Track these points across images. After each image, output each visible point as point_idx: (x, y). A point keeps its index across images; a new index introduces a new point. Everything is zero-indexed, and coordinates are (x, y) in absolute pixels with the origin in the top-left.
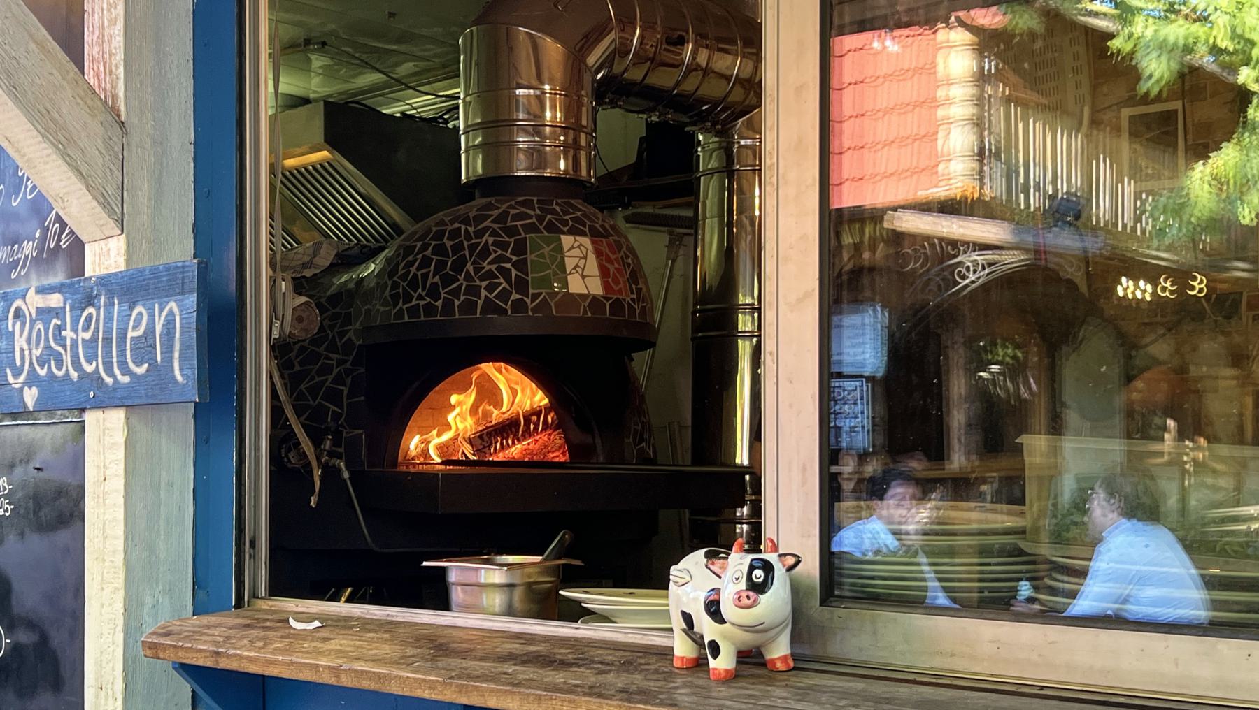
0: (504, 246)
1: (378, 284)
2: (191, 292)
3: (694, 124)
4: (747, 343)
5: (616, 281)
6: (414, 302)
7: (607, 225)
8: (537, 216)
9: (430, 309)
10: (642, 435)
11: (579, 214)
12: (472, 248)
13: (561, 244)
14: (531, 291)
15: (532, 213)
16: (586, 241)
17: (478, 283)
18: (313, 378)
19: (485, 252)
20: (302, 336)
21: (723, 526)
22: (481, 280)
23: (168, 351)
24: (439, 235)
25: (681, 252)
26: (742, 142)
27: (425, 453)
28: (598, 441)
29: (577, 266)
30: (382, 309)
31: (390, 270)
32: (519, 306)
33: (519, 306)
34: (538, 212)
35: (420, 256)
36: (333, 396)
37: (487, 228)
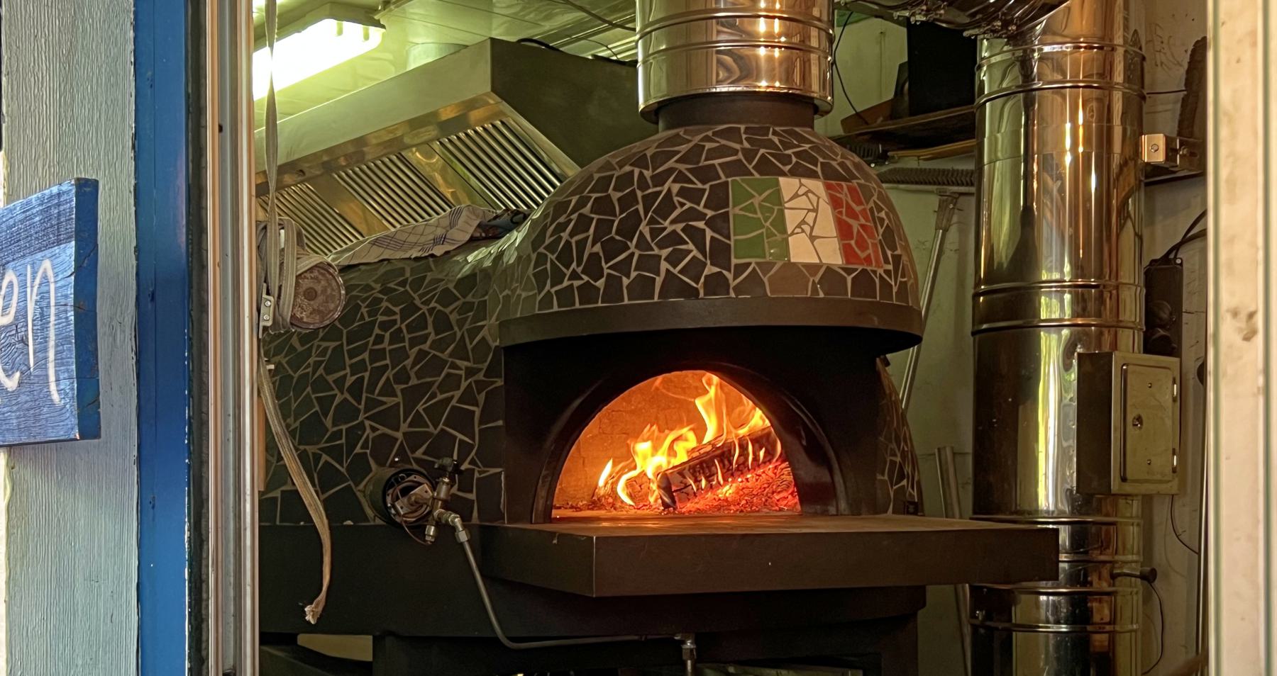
0: (694, 196)
1: (519, 258)
2: (68, 240)
3: (976, 25)
4: (1054, 336)
6: (566, 283)
7: (848, 163)
8: (744, 150)
10: (901, 468)
11: (807, 146)
12: (649, 200)
13: (778, 192)
14: (734, 261)
15: (737, 146)
16: (817, 186)
17: (656, 251)
18: (433, 396)
19: (667, 206)
21: (1024, 597)
22: (661, 247)
23: (42, 349)
24: (603, 184)
25: (955, 219)
26: (1047, 49)
28: (838, 478)
29: (803, 222)
30: (524, 295)
31: (535, 240)
32: (718, 284)
33: (718, 284)
34: (746, 145)
35: (575, 216)
36: (461, 420)
37: (671, 170)
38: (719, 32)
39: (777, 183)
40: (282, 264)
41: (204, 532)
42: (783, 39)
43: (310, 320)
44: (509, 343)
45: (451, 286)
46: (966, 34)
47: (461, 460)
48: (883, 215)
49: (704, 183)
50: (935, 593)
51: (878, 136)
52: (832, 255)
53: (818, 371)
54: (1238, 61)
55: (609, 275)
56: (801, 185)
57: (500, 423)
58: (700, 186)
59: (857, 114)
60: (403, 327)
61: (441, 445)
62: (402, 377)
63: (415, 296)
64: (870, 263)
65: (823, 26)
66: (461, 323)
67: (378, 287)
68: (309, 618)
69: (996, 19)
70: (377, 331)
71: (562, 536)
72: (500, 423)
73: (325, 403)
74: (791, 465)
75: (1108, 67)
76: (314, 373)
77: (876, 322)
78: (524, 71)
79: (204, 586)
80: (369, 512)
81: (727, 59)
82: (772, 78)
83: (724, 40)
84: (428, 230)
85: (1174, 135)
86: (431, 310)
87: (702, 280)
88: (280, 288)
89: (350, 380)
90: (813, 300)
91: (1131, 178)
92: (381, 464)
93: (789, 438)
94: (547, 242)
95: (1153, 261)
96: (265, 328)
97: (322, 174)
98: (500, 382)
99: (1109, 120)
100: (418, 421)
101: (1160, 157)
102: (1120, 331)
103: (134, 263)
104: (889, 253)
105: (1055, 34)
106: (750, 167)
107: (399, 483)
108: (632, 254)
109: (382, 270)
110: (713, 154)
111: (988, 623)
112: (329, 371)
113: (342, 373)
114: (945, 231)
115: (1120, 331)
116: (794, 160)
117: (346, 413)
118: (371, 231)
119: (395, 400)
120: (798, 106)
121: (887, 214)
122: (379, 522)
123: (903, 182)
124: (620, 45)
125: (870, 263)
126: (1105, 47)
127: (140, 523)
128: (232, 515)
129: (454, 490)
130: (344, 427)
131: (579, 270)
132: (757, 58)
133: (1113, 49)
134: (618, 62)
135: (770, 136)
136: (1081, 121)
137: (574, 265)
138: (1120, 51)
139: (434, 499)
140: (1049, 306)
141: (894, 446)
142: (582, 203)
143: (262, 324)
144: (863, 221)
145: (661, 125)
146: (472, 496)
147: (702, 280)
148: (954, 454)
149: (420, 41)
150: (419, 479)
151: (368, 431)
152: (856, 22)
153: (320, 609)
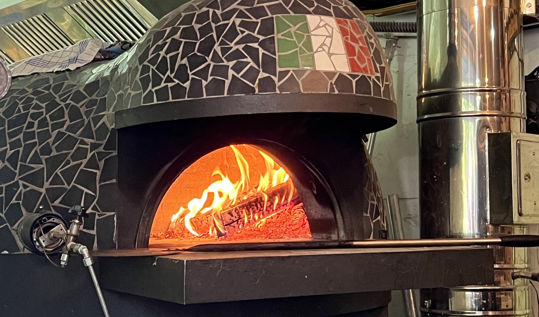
0: (251, 26)
1: (130, 69)
6: (163, 85)
12: (220, 30)
13: (306, 25)
14: (278, 69)
16: (331, 21)
17: (226, 63)
18: (68, 163)
24: (188, 19)
25: (396, 53)
29: (323, 44)
30: (133, 93)
35: (169, 40)
36: (88, 179)
37: (235, 10)
39: (306, 19)
44: (122, 126)
45: (81, 89)
47: (86, 207)
48: (372, 41)
49: (257, 18)
52: (343, 66)
53: (325, 144)
55: (192, 78)
56: (321, 20)
57: (114, 181)
58: (254, 20)
60: (47, 116)
61: (72, 197)
62: (46, 150)
63: (56, 96)
64: (367, 72)
66: (88, 114)
67: (31, 91)
70: (29, 119)
72: (114, 181)
77: (371, 111)
80: (21, 245)
86: (67, 106)
87: (257, 82)
89: (10, 153)
90: (330, 95)
91: (515, 26)
92: (29, 210)
94: (150, 57)
98: (115, 153)
102: (512, 119)
104: (378, 65)
106: (288, 8)
108: (209, 65)
109: (33, 80)
111: (434, 311)
115: (512, 119)
119: (42, 166)
121: (375, 41)
122: (27, 251)
125: (367, 72)
131: (172, 76)
137: (168, 73)
139: (68, 235)
141: (372, 194)
142: (174, 32)
144: (361, 44)
146: (94, 232)
147: (257, 82)
148: (399, 199)
150: (56, 220)
151: (21, 188)
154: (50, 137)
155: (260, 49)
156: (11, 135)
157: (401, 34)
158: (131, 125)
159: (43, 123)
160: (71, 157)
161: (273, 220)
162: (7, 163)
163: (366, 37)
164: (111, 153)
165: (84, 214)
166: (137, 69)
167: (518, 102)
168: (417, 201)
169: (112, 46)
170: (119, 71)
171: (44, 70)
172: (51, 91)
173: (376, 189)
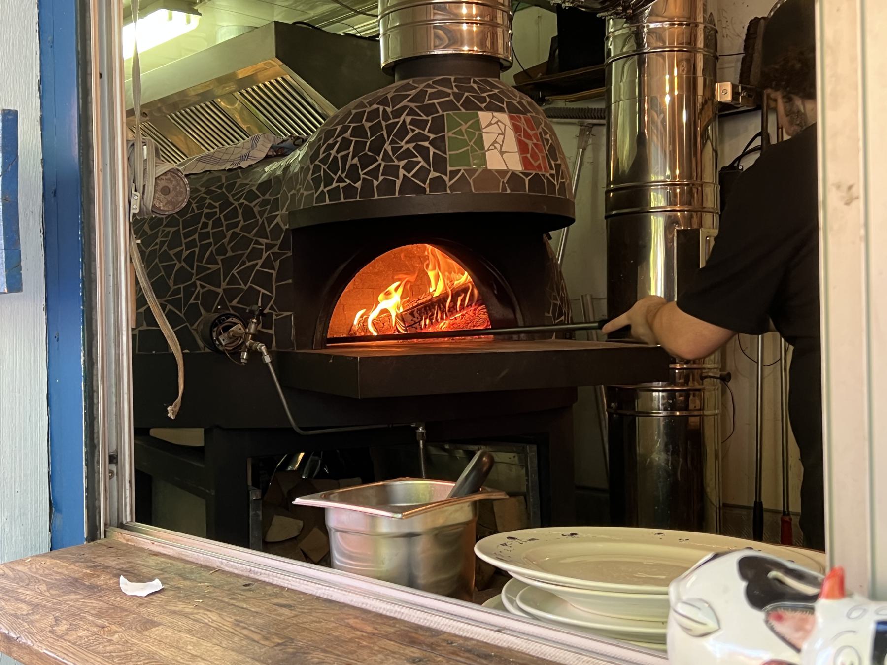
0: (421, 124)
1: (301, 168)
5: (534, 156)
6: (334, 185)
9: (350, 191)
11: (496, 91)
12: (390, 128)
13: (478, 122)
14: (449, 169)
15: (450, 91)
16: (504, 117)
17: (396, 163)
18: (244, 263)
19: (403, 132)
20: (169, 210)
22: (399, 159)
24: (358, 117)
25: (590, 141)
26: (652, 26)
27: (364, 327)
29: (495, 142)
30: (305, 193)
31: (313, 156)
32: (438, 184)
33: (438, 184)
34: (456, 90)
35: (339, 139)
36: (264, 280)
37: (404, 108)
38: (435, 14)
39: (477, 116)
40: (145, 170)
41: (94, 357)
42: (479, 18)
43: (165, 209)
44: (295, 226)
45: (254, 188)
46: (598, 16)
47: (264, 307)
48: (548, 137)
49: (427, 116)
50: (584, 392)
51: (539, 86)
52: (515, 164)
53: (503, 241)
54: (838, 10)
55: (364, 179)
56: (493, 117)
57: (290, 281)
58: (425, 118)
59: (524, 71)
60: (221, 216)
61: (250, 296)
62: (222, 250)
63: (229, 195)
64: (540, 169)
65: (506, 9)
66: (261, 213)
67: (203, 189)
68: (170, 415)
69: (619, 5)
70: (203, 219)
71: (336, 357)
72: (290, 281)
73: (169, 269)
74: (487, 307)
75: (693, 39)
76: (160, 249)
77: (545, 210)
78: (296, 43)
79: (95, 394)
80: (201, 344)
81: (441, 32)
82: (471, 44)
83: (438, 19)
84: (236, 151)
85: (737, 82)
86: (241, 205)
87: (428, 181)
88: (144, 186)
89: (185, 253)
90: (503, 195)
91: (709, 112)
92: (208, 310)
93: (484, 289)
94: (321, 156)
95: (724, 168)
96: (134, 215)
97: (163, 116)
98: (290, 254)
99: (695, 72)
100: (233, 281)
101: (728, 98)
102: (704, 214)
103: (41, 170)
104: (553, 163)
105: (657, 16)
106: (459, 105)
107: (221, 323)
108: (380, 164)
109: (205, 179)
110: (433, 96)
111: (620, 412)
112: (170, 247)
113: (180, 249)
114: (584, 150)
115: (704, 214)
116: (488, 100)
117: (183, 275)
118: (198, 153)
119: (218, 266)
120: (489, 64)
121: (551, 136)
122: (207, 350)
123: (555, 117)
124: (361, 26)
125: (540, 169)
126: (692, 24)
127: (49, 352)
128: (113, 345)
129: (259, 327)
130: (182, 286)
131: (343, 176)
132: (461, 31)
133: (697, 26)
134: (361, 37)
135: (472, 84)
136: (676, 74)
137: (340, 172)
138: (701, 26)
139: (246, 334)
140: (656, 199)
141: (555, 293)
142: (344, 130)
143: (132, 212)
144: (535, 141)
145: (396, 77)
146: (272, 332)
147: (428, 181)
148: (592, 299)
149: (224, 24)
150: (235, 320)
151: (199, 288)
152: (522, 9)
153: (177, 409)
154: (225, 237)
155: (431, 148)
156: (187, 236)
157: (595, 121)
158: (305, 225)
159: (217, 223)
160: (247, 257)
161: (457, 321)
162: (183, 264)
163: (540, 133)
164: (285, 254)
165: (261, 313)
166: (308, 168)
167: (711, 197)
168: (605, 301)
169: (284, 141)
170: (291, 169)
171: (216, 168)
172: (224, 190)
173: (559, 287)
